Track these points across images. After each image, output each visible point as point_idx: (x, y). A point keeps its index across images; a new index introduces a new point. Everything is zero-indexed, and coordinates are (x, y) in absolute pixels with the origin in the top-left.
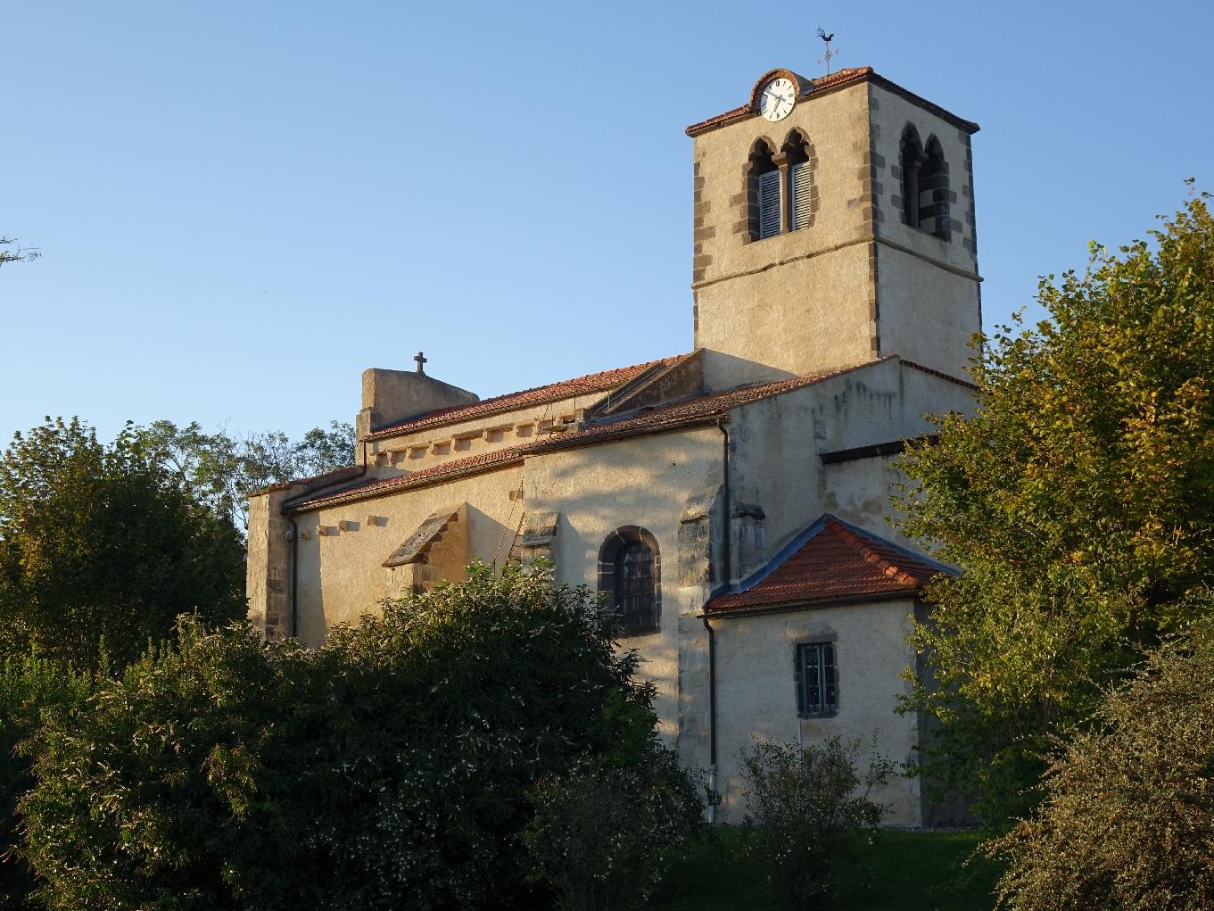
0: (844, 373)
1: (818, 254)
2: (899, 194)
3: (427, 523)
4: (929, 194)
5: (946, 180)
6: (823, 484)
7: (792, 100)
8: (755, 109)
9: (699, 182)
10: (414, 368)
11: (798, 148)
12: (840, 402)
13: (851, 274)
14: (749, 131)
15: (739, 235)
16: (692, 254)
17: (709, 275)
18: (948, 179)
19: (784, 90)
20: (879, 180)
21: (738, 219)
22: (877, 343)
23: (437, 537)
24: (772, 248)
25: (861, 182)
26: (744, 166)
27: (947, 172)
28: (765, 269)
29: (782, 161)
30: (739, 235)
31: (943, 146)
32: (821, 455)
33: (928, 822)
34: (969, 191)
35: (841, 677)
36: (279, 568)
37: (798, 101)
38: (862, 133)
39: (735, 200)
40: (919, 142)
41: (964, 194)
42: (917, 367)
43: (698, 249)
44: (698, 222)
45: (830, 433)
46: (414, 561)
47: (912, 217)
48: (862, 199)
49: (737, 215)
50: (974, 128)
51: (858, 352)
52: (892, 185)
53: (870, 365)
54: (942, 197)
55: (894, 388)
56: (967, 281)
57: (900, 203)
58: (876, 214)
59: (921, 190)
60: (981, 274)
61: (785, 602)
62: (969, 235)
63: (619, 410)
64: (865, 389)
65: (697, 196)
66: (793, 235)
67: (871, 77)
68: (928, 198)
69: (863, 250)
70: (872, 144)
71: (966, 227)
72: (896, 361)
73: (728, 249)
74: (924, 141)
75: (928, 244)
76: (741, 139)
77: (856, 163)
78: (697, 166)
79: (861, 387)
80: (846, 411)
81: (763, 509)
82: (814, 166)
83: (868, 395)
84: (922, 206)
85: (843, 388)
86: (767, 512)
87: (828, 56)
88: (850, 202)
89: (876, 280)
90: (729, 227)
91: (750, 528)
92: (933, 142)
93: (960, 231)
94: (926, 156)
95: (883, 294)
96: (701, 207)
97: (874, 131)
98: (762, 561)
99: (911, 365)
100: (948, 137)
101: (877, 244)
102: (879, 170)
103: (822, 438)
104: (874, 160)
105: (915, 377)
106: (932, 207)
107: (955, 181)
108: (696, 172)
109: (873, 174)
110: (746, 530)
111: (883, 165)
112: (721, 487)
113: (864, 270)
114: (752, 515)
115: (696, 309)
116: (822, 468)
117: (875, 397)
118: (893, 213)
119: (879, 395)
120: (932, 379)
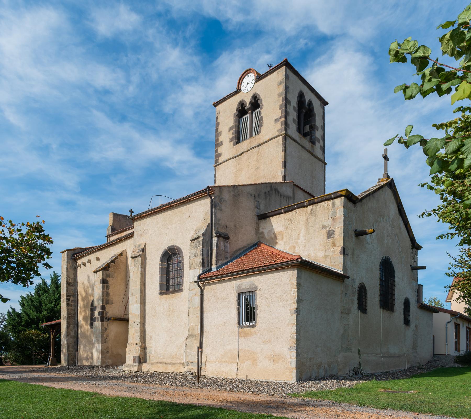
2: (296, 119)
4: (308, 126)
5: (315, 120)
6: (258, 228)
7: (254, 81)
8: (238, 91)
9: (218, 124)
11: (256, 103)
12: (267, 194)
14: (235, 100)
15: (232, 143)
18: (315, 120)
19: (251, 78)
20: (288, 110)
22: (284, 177)
24: (244, 145)
25: (281, 110)
26: (234, 114)
27: (315, 117)
29: (249, 109)
30: (232, 143)
31: (314, 106)
32: (257, 216)
35: (258, 308)
36: (71, 277)
37: (256, 82)
38: (282, 89)
39: (231, 129)
40: (305, 100)
41: (321, 128)
42: (300, 188)
45: (262, 207)
48: (280, 118)
50: (326, 103)
52: (293, 115)
53: (281, 183)
54: (313, 127)
55: (291, 194)
56: (321, 163)
57: (296, 123)
58: (286, 124)
59: (305, 125)
60: (326, 161)
61: (233, 272)
62: (322, 145)
64: (278, 192)
66: (252, 139)
68: (307, 128)
69: (281, 139)
71: (321, 142)
72: (292, 184)
76: (231, 106)
77: (280, 102)
79: (277, 191)
80: (269, 199)
81: (229, 235)
83: (280, 195)
84: (305, 132)
85: (269, 189)
86: (231, 237)
89: (285, 152)
90: (228, 140)
92: (310, 103)
93: (319, 142)
94: (307, 107)
95: (288, 157)
96: (218, 134)
98: (227, 258)
99: (298, 187)
100: (316, 104)
101: (286, 137)
102: (288, 106)
103: (259, 209)
104: (286, 101)
106: (309, 132)
107: (318, 123)
109: (286, 107)
110: (220, 243)
111: (290, 105)
112: (209, 224)
113: (281, 148)
114: (224, 238)
115: (215, 175)
116: (258, 222)
117: (282, 197)
118: (293, 127)
119: (284, 196)
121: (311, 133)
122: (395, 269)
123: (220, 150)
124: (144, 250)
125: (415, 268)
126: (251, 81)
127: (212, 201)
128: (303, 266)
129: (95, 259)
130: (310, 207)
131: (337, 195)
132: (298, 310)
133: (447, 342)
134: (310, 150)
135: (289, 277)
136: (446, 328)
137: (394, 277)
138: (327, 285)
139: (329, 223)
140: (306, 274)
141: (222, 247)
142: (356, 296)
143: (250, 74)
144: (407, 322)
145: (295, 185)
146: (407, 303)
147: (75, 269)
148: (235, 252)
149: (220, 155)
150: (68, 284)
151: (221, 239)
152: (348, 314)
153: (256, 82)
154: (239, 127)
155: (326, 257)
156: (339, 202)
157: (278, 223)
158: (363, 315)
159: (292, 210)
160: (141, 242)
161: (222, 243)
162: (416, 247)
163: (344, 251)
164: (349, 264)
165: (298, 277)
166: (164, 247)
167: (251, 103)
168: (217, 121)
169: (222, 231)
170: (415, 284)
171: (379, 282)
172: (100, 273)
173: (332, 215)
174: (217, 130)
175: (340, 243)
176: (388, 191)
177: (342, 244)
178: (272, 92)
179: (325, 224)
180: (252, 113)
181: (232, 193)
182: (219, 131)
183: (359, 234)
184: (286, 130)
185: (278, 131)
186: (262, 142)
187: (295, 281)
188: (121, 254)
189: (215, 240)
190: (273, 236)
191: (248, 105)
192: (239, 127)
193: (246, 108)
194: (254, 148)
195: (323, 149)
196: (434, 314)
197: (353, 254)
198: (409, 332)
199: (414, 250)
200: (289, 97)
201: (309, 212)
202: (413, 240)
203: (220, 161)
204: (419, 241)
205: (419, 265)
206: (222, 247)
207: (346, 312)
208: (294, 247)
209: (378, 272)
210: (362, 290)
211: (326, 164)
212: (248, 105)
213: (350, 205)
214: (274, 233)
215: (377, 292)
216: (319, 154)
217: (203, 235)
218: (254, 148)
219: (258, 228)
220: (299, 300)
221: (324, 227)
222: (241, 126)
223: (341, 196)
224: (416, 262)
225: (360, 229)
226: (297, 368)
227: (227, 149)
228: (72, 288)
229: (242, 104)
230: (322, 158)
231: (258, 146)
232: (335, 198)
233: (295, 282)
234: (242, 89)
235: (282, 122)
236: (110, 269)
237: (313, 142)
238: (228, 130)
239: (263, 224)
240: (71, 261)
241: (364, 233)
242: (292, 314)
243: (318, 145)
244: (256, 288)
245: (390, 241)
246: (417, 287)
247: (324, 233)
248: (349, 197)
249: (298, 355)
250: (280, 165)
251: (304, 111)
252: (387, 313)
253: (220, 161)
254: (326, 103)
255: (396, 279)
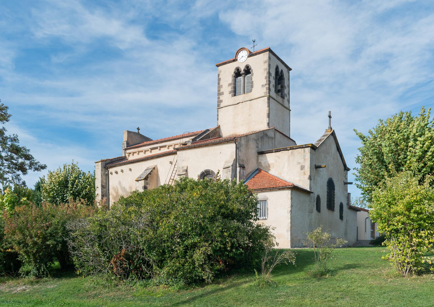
0: (263, 131)
1: (253, 100)
3: (146, 170)
4: (280, 86)
7: (247, 56)
9: (219, 80)
10: (136, 131)
11: (248, 71)
12: (262, 138)
13: (262, 106)
15: (231, 95)
16: (217, 100)
17: (222, 105)
19: (243, 55)
20: (270, 80)
21: (230, 90)
22: (268, 124)
23: (150, 174)
24: (240, 98)
28: (238, 104)
29: (243, 74)
30: (231, 95)
33: (292, 247)
34: (289, 86)
37: (248, 57)
38: (266, 66)
39: (230, 85)
43: (219, 98)
44: (219, 90)
45: (260, 147)
46: (144, 179)
47: (277, 91)
48: (266, 85)
49: (230, 89)
50: (290, 69)
51: (264, 127)
52: (273, 82)
54: (283, 87)
55: (273, 136)
58: (269, 89)
59: (278, 85)
60: (290, 109)
63: (200, 140)
65: (219, 83)
67: (270, 50)
68: (279, 87)
69: (266, 99)
70: (269, 70)
71: (288, 96)
72: (274, 129)
73: (227, 98)
74: (280, 71)
75: (280, 99)
76: (230, 69)
77: (265, 74)
78: (219, 75)
79: (266, 135)
82: (252, 75)
85: (263, 135)
87: (254, 46)
88: (262, 86)
91: (242, 170)
92: (282, 71)
95: (270, 111)
96: (220, 87)
97: (269, 65)
99: (277, 130)
101: (270, 97)
104: (269, 73)
105: (278, 134)
107: (286, 84)
108: (219, 76)
111: (271, 76)
113: (266, 105)
118: (273, 89)
120: (281, 135)
121: (282, 91)
122: (335, 185)
123: (221, 98)
124: (186, 171)
125: (346, 183)
126: (245, 56)
127: (236, 146)
128: (295, 189)
129: (128, 170)
130: (290, 151)
131: (306, 146)
132: (291, 211)
133: (366, 231)
134: (282, 103)
135: (287, 194)
136: (366, 222)
137: (334, 189)
138: (303, 197)
139: (302, 161)
140: (295, 192)
141: (242, 173)
142: (316, 202)
143: (244, 51)
144: (341, 217)
145: (276, 130)
146: (341, 206)
147: (107, 175)
148: (247, 175)
149: (221, 101)
150: (102, 186)
151: (241, 168)
152: (311, 213)
153: (248, 57)
154: (235, 84)
155: (300, 180)
156: (308, 150)
157: (270, 158)
158: (319, 213)
159: (280, 151)
160: (183, 165)
161: (242, 170)
162: (347, 169)
163: (310, 178)
164: (312, 184)
165: (291, 194)
166: (202, 170)
167: (244, 70)
168: (219, 76)
169: (241, 163)
170: (346, 193)
171: (326, 194)
172: (143, 182)
173: (304, 157)
174: (219, 83)
175: (308, 173)
176: (332, 137)
177: (309, 174)
178: (260, 67)
179: (299, 161)
180: (245, 77)
181: (246, 140)
182: (221, 84)
183: (318, 167)
184: (269, 93)
185: (264, 93)
186: (253, 98)
187: (290, 196)
188: (154, 168)
189: (238, 169)
190: (267, 165)
191: (242, 71)
192: (235, 84)
193: (241, 73)
194: (247, 101)
195: (289, 101)
196: (358, 212)
197: (314, 179)
198: (342, 224)
199: (346, 171)
200: (271, 72)
201: (290, 154)
202: (345, 165)
203: (221, 106)
204: (348, 166)
205: (349, 181)
206: (242, 173)
207: (311, 212)
208: (281, 173)
209: (326, 187)
210: (318, 198)
211: (290, 110)
212: (242, 71)
213: (313, 151)
214: (268, 164)
215: (326, 200)
216: (287, 106)
217: (232, 166)
218: (247, 101)
219: (258, 160)
220: (292, 206)
221: (299, 163)
222: (237, 84)
223: (309, 147)
224: (347, 179)
225: (317, 164)
226: (291, 241)
227: (227, 98)
228: (105, 190)
229: (238, 69)
230: (288, 107)
231: (250, 100)
232: (305, 147)
233: (290, 197)
234: (238, 59)
235: (267, 88)
236: (148, 179)
237: (283, 97)
238: (227, 85)
239: (261, 157)
240: (103, 169)
241: (320, 167)
242: (288, 213)
243: (286, 98)
244: (268, 199)
245: (333, 168)
246: (347, 195)
247: (299, 167)
248: (313, 148)
249: (291, 234)
250: (266, 115)
251: (278, 77)
252: (331, 212)
253: (221, 106)
254: (290, 69)
255: (336, 191)
